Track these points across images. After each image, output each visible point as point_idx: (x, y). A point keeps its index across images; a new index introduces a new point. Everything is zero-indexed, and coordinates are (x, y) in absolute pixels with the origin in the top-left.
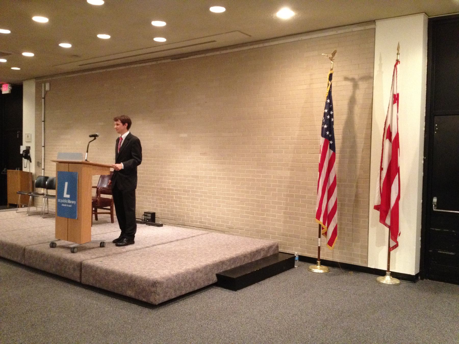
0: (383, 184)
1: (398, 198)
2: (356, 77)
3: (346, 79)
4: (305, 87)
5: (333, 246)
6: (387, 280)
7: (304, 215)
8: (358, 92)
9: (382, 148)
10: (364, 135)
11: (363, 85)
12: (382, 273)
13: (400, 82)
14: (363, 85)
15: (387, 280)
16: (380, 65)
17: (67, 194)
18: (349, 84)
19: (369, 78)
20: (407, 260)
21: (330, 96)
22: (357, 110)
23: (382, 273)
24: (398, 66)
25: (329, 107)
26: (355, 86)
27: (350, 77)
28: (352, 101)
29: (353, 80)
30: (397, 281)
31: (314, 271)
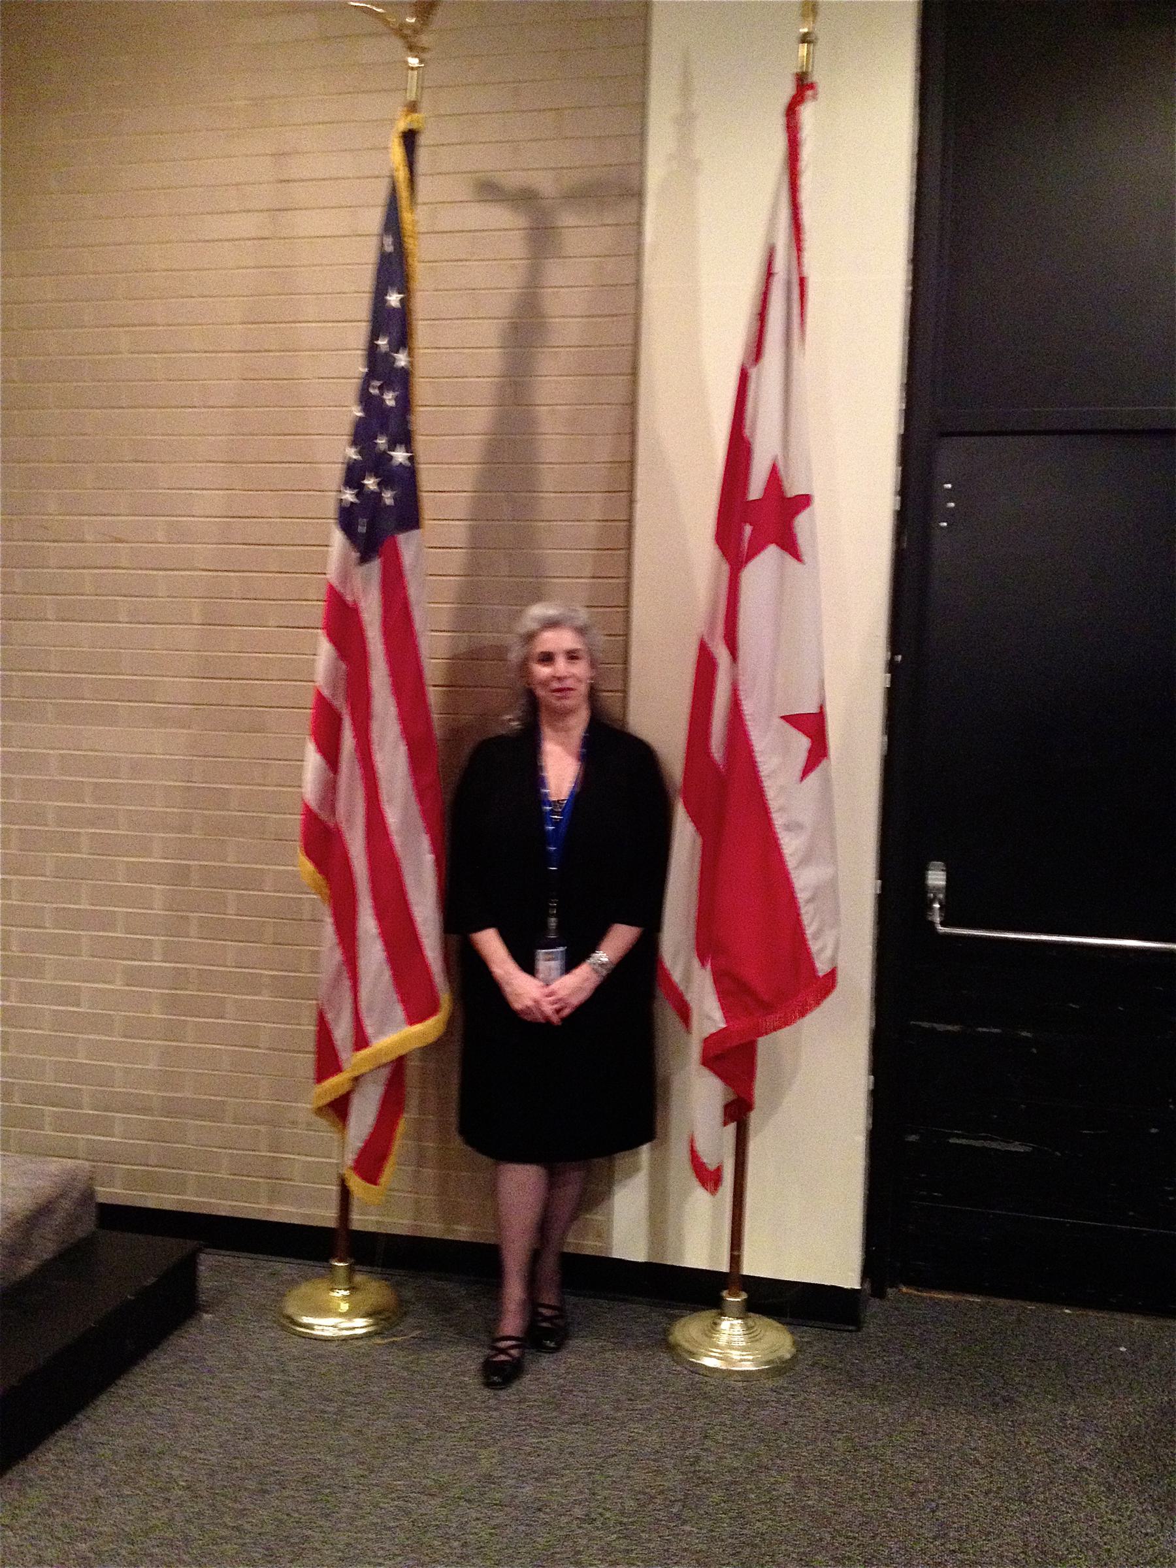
0: (446, 958)
1: (836, 948)
2: (545, 183)
3: (489, 191)
4: (246, 225)
5: (383, 1180)
6: (731, 1345)
8: (556, 273)
9: (804, 196)
10: (591, 528)
11: (583, 235)
12: (702, 1292)
13: (779, 276)
14: (583, 235)
15: (731, 1345)
16: (685, 121)
18: (502, 217)
19: (618, 192)
20: (811, 1225)
21: (393, 269)
22: (555, 385)
23: (702, 1292)
24: (808, 113)
25: (392, 325)
26: (542, 238)
27: (513, 180)
28: (525, 328)
29: (524, 199)
30: (778, 1340)
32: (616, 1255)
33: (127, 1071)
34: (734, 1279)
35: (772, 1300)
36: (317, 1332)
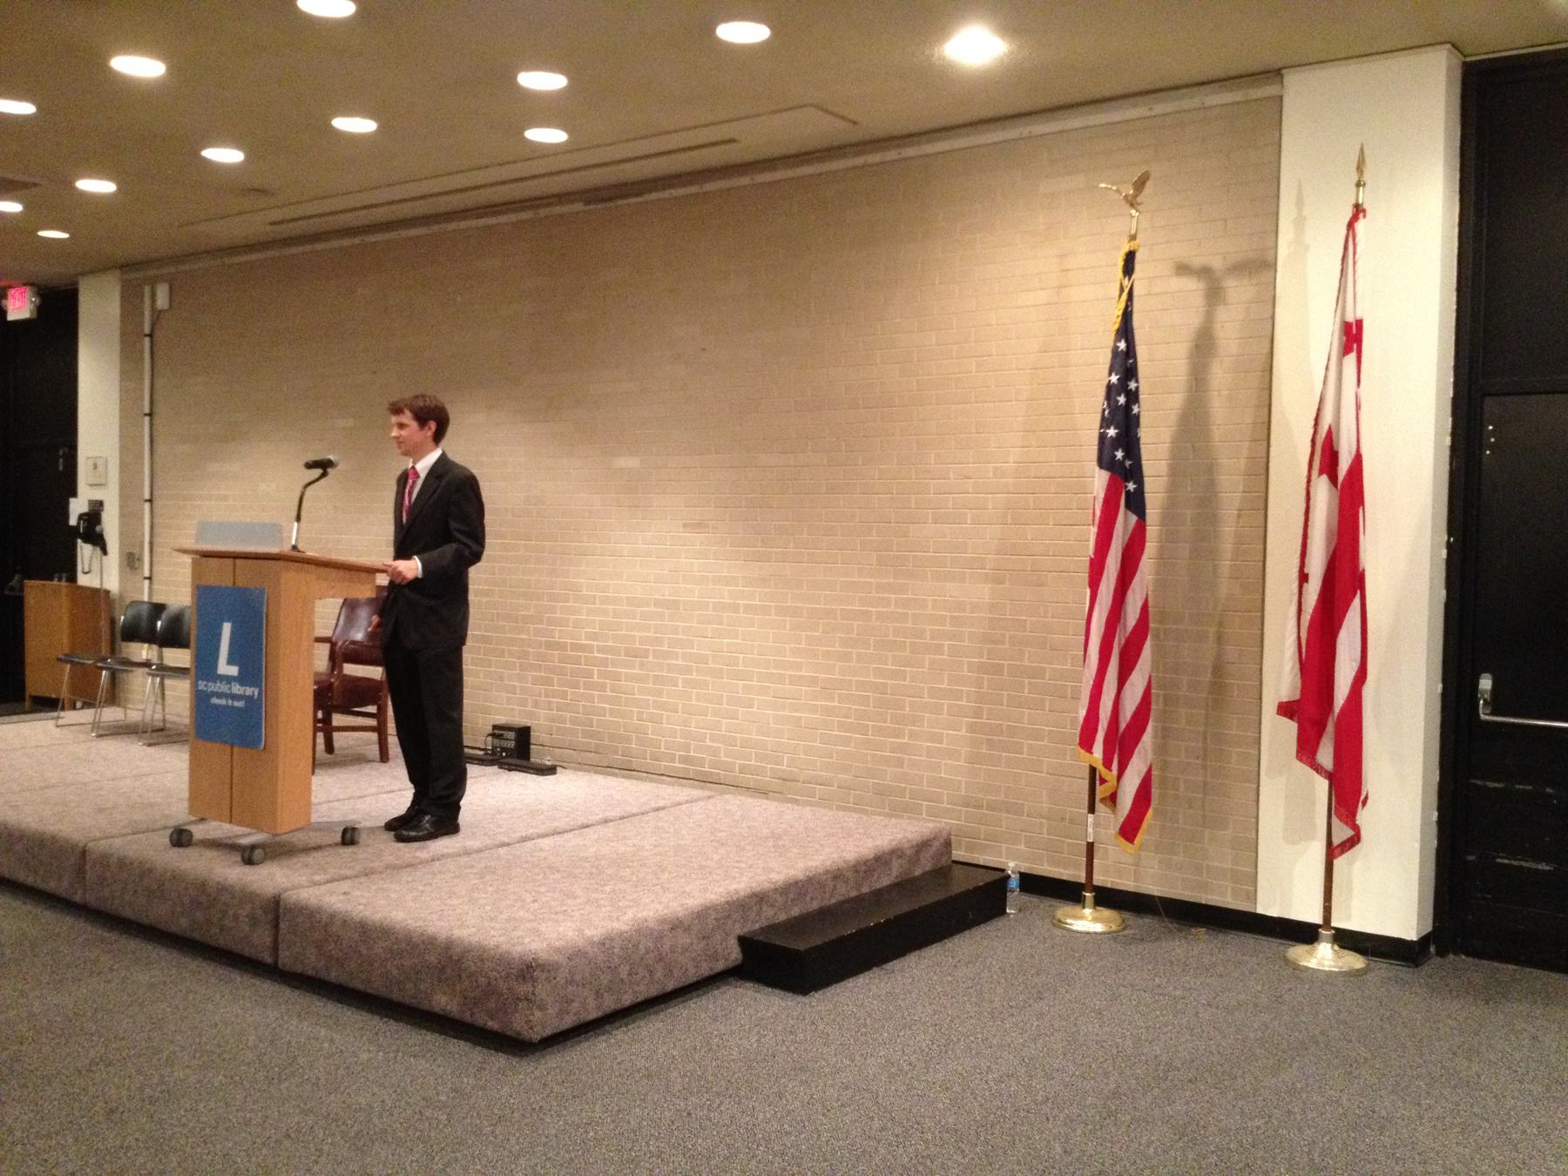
2: (1217, 263)
3: (1183, 269)
4: (1042, 297)
7: (1037, 735)
8: (1222, 314)
9: (1304, 505)
10: (1243, 462)
11: (1238, 291)
12: (1305, 934)
13: (1366, 281)
14: (1238, 291)
16: (1300, 222)
18: (1193, 287)
19: (1261, 266)
20: (1389, 889)
21: (1126, 330)
22: (1220, 374)
23: (1305, 934)
25: (1125, 364)
26: (1214, 295)
27: (1197, 262)
28: (1203, 346)
29: (1205, 272)
30: (1356, 961)
32: (1260, 910)
33: (874, 756)
34: (1089, 885)
35: (1348, 940)
36: (1074, 928)
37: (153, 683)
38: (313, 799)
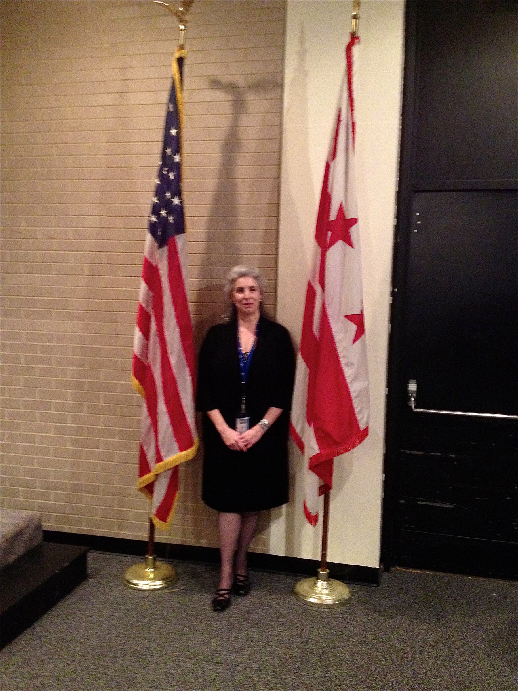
2: (240, 81)
3: (215, 84)
4: (108, 99)
6: (322, 593)
7: (111, 434)
8: (245, 120)
9: (354, 86)
10: (260, 233)
11: (257, 103)
12: (309, 569)
13: (343, 122)
14: (257, 103)
15: (322, 593)
16: (302, 54)
17: (233, 426)
18: (221, 96)
19: (272, 85)
20: (357, 540)
21: (173, 119)
22: (244, 170)
23: (309, 569)
25: (172, 143)
26: (239, 105)
27: (226, 79)
28: (231, 145)
29: (231, 88)
30: (342, 591)
31: (140, 587)
32: (271, 553)
34: (323, 564)
35: (340, 573)
37: (145, 537)
38: (282, 554)
